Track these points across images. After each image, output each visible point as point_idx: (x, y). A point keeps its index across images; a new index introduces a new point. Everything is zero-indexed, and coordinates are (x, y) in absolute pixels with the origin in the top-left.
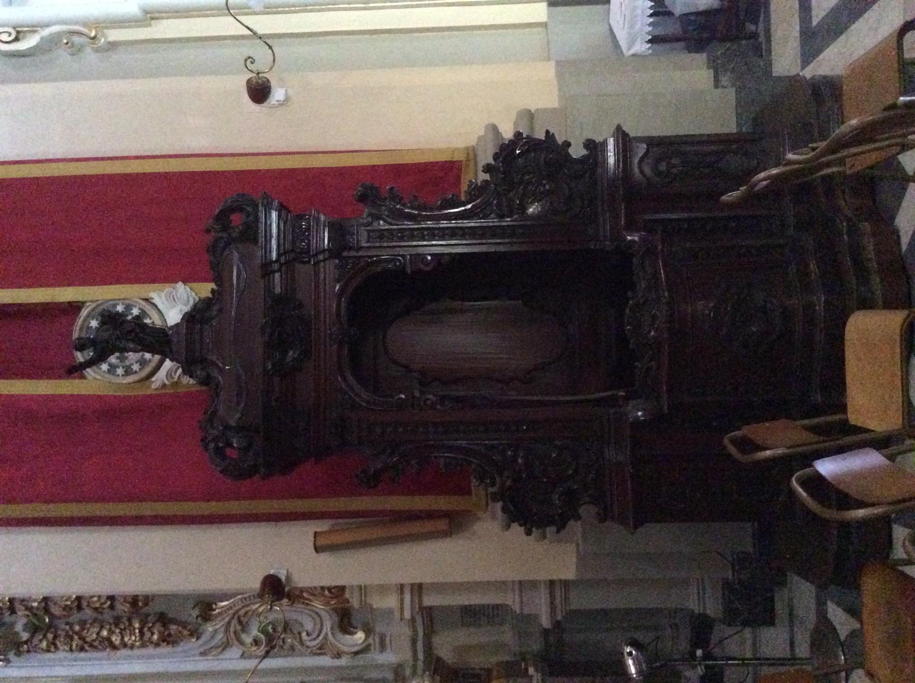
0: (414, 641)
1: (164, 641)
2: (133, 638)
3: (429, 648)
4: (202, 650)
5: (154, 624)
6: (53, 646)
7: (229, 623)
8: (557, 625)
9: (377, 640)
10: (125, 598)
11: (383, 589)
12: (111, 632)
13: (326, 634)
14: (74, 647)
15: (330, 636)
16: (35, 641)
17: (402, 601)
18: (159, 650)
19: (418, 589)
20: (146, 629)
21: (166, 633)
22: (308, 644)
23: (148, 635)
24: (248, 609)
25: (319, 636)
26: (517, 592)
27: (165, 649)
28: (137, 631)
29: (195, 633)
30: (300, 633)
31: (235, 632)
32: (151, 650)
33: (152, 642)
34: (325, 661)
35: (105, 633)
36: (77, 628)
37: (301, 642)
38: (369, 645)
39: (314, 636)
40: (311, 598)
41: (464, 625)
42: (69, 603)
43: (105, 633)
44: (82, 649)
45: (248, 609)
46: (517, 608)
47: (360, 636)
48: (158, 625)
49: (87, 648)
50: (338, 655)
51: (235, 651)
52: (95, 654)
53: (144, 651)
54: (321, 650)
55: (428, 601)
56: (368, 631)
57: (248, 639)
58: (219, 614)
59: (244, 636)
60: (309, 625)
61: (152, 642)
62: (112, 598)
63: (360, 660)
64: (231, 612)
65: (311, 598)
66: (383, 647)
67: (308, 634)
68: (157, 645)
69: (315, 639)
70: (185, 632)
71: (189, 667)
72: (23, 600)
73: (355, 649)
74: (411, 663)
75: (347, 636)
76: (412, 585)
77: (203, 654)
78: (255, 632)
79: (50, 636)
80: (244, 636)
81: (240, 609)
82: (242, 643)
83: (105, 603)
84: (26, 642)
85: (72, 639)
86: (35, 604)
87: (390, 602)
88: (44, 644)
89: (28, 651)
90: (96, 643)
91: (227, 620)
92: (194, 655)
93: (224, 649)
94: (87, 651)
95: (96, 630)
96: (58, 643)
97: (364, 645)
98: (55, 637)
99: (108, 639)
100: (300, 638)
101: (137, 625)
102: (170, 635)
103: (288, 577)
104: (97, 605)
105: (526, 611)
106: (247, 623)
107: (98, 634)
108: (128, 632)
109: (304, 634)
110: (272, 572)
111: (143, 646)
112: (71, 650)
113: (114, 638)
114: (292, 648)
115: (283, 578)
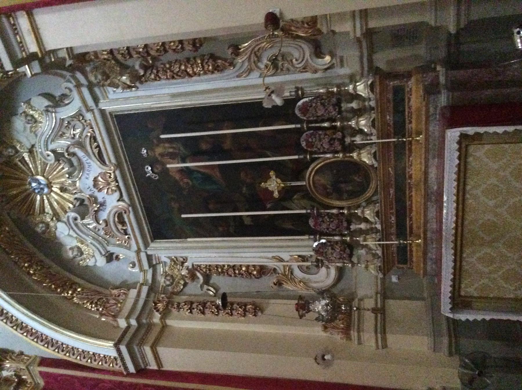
0: (361, 57)
1: (215, 70)
2: (199, 69)
3: (370, 61)
4: (237, 74)
5: (208, 60)
6: (157, 78)
7: (250, 56)
8: (458, 33)
9: (338, 60)
10: (188, 41)
11: (341, 16)
12: (186, 67)
13: (307, 60)
14: (168, 77)
15: (310, 60)
16: (148, 75)
17: (355, 27)
18: (214, 76)
19: (365, 14)
20: (205, 63)
21: (216, 65)
22: (297, 66)
23: (206, 67)
24: (259, 46)
25: (303, 60)
26: (433, 14)
27: (216, 75)
28: (200, 65)
29: (232, 64)
30: (291, 61)
31: (254, 62)
32: (210, 76)
33: (209, 71)
34: (308, 75)
35: (183, 67)
36: (168, 66)
37: (293, 66)
38: (334, 64)
39: (300, 61)
40: (296, 30)
41: (393, 46)
42: (159, 47)
43: (183, 67)
44: (173, 78)
45: (259, 46)
46: (433, 23)
47: (328, 58)
48: (211, 61)
49: (176, 77)
50: (316, 71)
51: (255, 74)
52: (179, 81)
53: (206, 77)
54: (305, 69)
55: (372, 24)
56: (333, 55)
57: (262, 66)
58: (244, 51)
59: (260, 64)
60: (296, 54)
61: (209, 71)
62: (181, 42)
63: (329, 73)
64: (250, 49)
65: (296, 30)
66: (342, 66)
67: (296, 60)
68: (213, 73)
69: (299, 64)
70: (227, 64)
71: (233, 83)
72: (134, 49)
73: (326, 67)
74: (360, 72)
75: (320, 60)
76: (361, 11)
77: (238, 76)
78: (265, 61)
79: (155, 71)
80: (260, 64)
81: (255, 47)
82: (258, 68)
83: (177, 46)
84: (143, 76)
85: (167, 72)
86: (141, 50)
87: (347, 27)
88: (153, 76)
89: (146, 81)
90: (179, 74)
91: (248, 54)
92: (234, 77)
93: (249, 73)
94: (176, 79)
95: (178, 66)
96: (160, 75)
97: (330, 64)
98: (158, 72)
99: (186, 71)
100: (292, 63)
101: (199, 62)
102: (218, 66)
103: (281, 13)
104: (174, 48)
105: (438, 24)
106: (260, 55)
107: (179, 68)
108: (195, 65)
109: (294, 60)
110: (271, 11)
111: (205, 73)
112: (167, 78)
113: (188, 70)
114: (288, 70)
115: (278, 14)
